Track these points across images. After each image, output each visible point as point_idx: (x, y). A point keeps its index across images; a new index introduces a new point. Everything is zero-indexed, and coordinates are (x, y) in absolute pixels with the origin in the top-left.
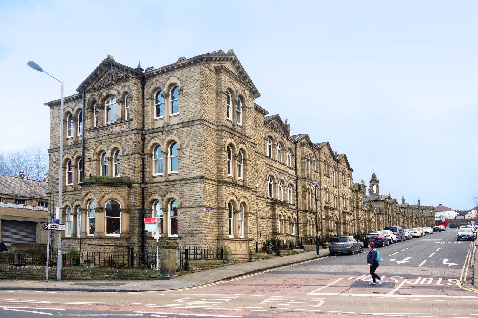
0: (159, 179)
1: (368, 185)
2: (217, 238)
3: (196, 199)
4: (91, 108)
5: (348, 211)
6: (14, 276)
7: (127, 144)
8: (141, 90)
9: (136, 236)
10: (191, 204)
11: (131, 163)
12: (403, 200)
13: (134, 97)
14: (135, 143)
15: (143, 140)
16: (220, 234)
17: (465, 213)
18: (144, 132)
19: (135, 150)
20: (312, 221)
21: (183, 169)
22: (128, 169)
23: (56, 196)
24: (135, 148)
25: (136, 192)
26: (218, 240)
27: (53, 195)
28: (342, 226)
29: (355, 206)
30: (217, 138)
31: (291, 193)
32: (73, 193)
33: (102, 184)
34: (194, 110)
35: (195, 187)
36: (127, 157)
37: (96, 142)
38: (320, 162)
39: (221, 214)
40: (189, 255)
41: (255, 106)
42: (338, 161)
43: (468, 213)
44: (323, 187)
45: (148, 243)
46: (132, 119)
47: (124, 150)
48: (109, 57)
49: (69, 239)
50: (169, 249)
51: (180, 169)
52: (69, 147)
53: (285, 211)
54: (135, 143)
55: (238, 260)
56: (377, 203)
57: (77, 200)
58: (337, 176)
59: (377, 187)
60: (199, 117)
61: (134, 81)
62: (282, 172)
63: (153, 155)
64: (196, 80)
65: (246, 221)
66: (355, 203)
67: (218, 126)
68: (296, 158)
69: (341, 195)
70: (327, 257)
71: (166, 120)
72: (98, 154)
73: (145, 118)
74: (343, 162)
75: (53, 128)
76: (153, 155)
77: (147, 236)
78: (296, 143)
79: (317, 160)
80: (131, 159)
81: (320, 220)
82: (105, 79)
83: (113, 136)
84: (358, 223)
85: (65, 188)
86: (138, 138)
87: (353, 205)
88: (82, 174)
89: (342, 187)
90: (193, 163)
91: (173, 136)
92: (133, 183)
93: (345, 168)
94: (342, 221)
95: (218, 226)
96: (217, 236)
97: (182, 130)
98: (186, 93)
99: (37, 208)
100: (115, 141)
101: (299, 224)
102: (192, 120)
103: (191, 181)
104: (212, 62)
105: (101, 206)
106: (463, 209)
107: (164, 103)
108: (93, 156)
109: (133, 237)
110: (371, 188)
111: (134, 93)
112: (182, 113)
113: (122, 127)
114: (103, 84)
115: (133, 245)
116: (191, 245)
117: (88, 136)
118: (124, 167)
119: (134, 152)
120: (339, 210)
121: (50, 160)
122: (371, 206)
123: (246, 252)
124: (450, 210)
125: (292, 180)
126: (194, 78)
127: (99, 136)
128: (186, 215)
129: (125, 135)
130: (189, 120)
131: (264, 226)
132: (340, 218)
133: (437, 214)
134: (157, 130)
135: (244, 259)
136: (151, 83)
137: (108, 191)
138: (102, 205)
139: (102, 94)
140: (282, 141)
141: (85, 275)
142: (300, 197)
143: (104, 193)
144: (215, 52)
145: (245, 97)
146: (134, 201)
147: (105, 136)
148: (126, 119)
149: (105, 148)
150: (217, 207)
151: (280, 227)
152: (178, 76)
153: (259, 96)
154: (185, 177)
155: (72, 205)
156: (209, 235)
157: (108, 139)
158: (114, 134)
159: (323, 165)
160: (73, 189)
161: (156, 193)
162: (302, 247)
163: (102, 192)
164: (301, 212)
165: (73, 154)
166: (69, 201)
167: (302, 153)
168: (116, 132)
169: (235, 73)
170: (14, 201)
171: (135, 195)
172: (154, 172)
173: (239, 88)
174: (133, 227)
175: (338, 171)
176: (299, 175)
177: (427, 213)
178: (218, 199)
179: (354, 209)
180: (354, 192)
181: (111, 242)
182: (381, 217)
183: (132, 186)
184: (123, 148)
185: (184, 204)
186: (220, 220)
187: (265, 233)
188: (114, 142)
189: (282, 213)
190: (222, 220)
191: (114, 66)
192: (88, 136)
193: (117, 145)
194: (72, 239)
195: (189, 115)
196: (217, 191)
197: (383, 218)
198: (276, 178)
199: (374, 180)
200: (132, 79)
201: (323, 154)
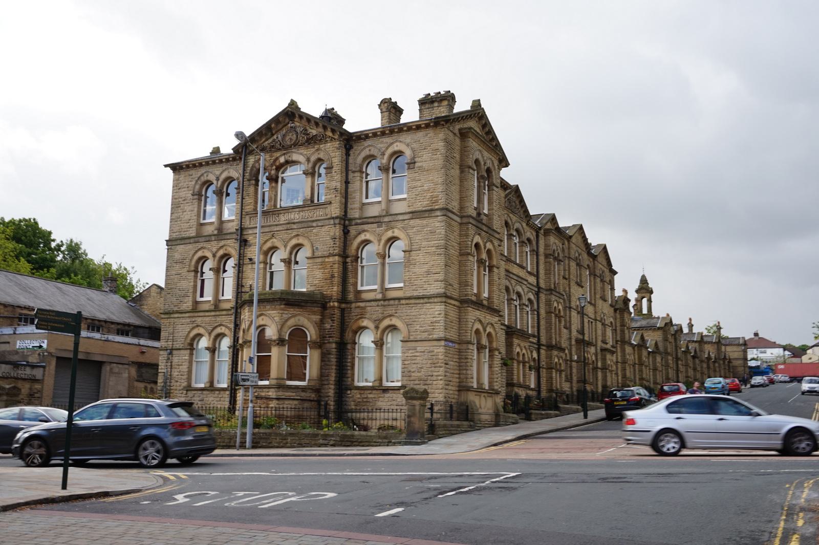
0: (371, 296)
1: (633, 296)
2: (457, 389)
5: (608, 346)
8: (345, 157)
9: (332, 384)
12: (691, 326)
13: (334, 169)
15: (346, 232)
16: (463, 382)
17: (803, 350)
18: (347, 222)
19: (334, 250)
20: (560, 364)
21: (412, 282)
23: (178, 318)
25: (334, 314)
26: (459, 391)
27: (172, 316)
28: (600, 374)
29: (619, 338)
30: (460, 235)
31: (530, 316)
32: (213, 313)
33: (284, 302)
35: (432, 310)
38: (569, 261)
39: (464, 351)
41: (501, 182)
42: (594, 257)
43: (808, 352)
44: (573, 305)
45: (350, 395)
48: (292, 101)
49: (202, 390)
51: (409, 282)
52: (207, 239)
53: (525, 347)
56: (650, 331)
57: (220, 325)
58: (593, 283)
59: (650, 301)
61: (337, 144)
62: (520, 280)
63: (359, 257)
65: (491, 363)
66: (618, 332)
67: (462, 217)
68: (537, 255)
69: (598, 319)
70: (516, 443)
71: (383, 205)
73: (349, 200)
74: (601, 259)
75: (176, 206)
76: (359, 257)
78: (537, 230)
79: (566, 257)
81: (569, 362)
82: (284, 136)
83: (295, 226)
84: (624, 369)
85: (194, 304)
86: (337, 231)
87: (616, 335)
89: (600, 303)
90: (428, 273)
91: (396, 230)
93: (605, 269)
94: (600, 365)
95: (460, 370)
96: (457, 384)
97: (412, 222)
98: (419, 167)
99: (106, 336)
100: (299, 233)
101: (541, 369)
103: (426, 300)
104: (456, 123)
105: (282, 337)
106: (797, 344)
110: (639, 304)
112: (412, 197)
113: (312, 213)
114: (280, 144)
115: (327, 399)
120: (596, 346)
122: (642, 338)
123: (491, 411)
124: (773, 345)
125: (532, 293)
126: (434, 146)
127: (268, 224)
128: (417, 352)
130: (424, 209)
132: (597, 359)
133: (752, 353)
134: (370, 220)
136: (362, 147)
139: (277, 159)
140: (521, 228)
141: (289, 440)
142: (543, 322)
143: (287, 316)
145: (493, 170)
146: (330, 329)
147: (281, 225)
150: (457, 339)
151: (519, 373)
152: (408, 140)
153: (507, 165)
154: (415, 294)
158: (297, 223)
159: (573, 264)
160: (212, 308)
161: (365, 318)
162: (557, 408)
163: (284, 316)
164: (544, 348)
166: (227, 327)
167: (547, 246)
169: (478, 130)
171: (332, 320)
172: (368, 285)
173: (487, 158)
175: (595, 275)
176: (542, 285)
177: (733, 353)
178: (460, 329)
179: (617, 343)
180: (618, 312)
181: (294, 394)
182: (659, 359)
183: (328, 305)
185: (412, 335)
186: (463, 360)
188: (298, 235)
189: (522, 350)
190: (466, 361)
194: (208, 390)
196: (459, 315)
197: (662, 360)
198: (512, 291)
199: (645, 289)
201: (574, 246)
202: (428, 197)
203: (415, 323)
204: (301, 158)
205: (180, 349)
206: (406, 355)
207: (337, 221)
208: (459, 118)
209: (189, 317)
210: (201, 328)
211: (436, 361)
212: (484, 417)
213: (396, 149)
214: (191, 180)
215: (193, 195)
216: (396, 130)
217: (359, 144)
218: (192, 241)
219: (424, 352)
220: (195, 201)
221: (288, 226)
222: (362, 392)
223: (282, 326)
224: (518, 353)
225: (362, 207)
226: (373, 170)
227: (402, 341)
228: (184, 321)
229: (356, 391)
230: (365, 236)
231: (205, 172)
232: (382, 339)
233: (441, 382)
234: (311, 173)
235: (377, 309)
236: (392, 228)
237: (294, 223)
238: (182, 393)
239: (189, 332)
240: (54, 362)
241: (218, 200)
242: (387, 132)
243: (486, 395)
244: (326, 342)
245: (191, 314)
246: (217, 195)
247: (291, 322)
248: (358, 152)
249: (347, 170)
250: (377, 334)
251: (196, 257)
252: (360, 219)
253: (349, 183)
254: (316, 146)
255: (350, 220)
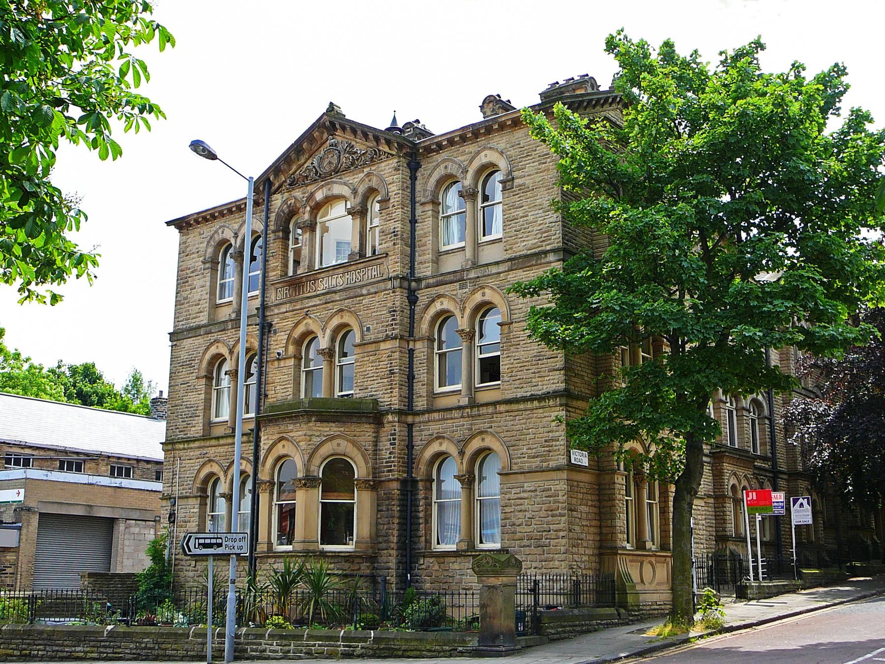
3: (547, 449)
4: (283, 231)
6: (119, 653)
7: (373, 314)
8: (409, 182)
9: (393, 549)
10: (535, 463)
11: (381, 363)
13: (391, 201)
14: (394, 311)
15: (412, 300)
19: (394, 329)
21: (513, 374)
22: (375, 378)
24: (392, 325)
34: (541, 227)
36: (372, 348)
37: (294, 313)
40: (540, 596)
45: (423, 567)
46: (387, 254)
47: (365, 329)
50: (500, 578)
53: (745, 476)
54: (394, 311)
55: (648, 608)
60: (553, 243)
61: (394, 162)
64: (545, 155)
71: (469, 253)
72: (299, 343)
75: (183, 280)
77: (419, 549)
80: (383, 352)
83: (337, 297)
86: (398, 299)
88: (262, 395)
91: (487, 291)
92: (387, 412)
98: (520, 186)
102: (537, 250)
107: (464, 212)
108: (286, 347)
109: (385, 552)
111: (394, 189)
112: (510, 234)
116: (536, 570)
117: (273, 297)
118: (364, 373)
119: (390, 333)
121: (173, 359)
129: (369, 294)
130: (529, 252)
131: (699, 517)
135: (663, 607)
136: (435, 164)
137: (328, 433)
138: (314, 471)
139: (312, 194)
141: (292, 647)
144: (573, 79)
146: (390, 458)
148: (369, 253)
149: (313, 327)
152: (502, 145)
154: (519, 395)
155: (226, 472)
156: (580, 542)
157: (323, 304)
161: (444, 438)
163: (314, 439)
164: (785, 477)
165: (233, 343)
168: (345, 286)
170: (58, 463)
174: (385, 527)
184: (361, 327)
185: (516, 464)
187: (702, 537)
188: (341, 310)
189: (740, 483)
191: (344, 129)
192: (273, 297)
193: (347, 318)
195: (529, 238)
200: (387, 157)
202: (535, 233)
203: (521, 443)
204: (346, 191)
205: (187, 497)
206: (507, 496)
207: (397, 283)
208: (582, 102)
209: (199, 447)
210: (214, 464)
211: (554, 506)
212: (647, 598)
213: (484, 160)
214: (201, 239)
215: (204, 263)
216: (482, 131)
217: (430, 160)
218: (202, 331)
219: (535, 491)
220: (207, 271)
221: (328, 296)
222: (442, 560)
223: (311, 456)
224: (734, 486)
225: (437, 259)
226: (452, 200)
227: (499, 474)
228: (192, 454)
229: (432, 560)
230: (442, 303)
231: (220, 228)
232: (471, 472)
233: (564, 541)
234: (360, 212)
235: (462, 421)
236: (482, 288)
237: (335, 292)
238: (190, 565)
239: (199, 471)
240: (35, 520)
241: (237, 266)
242: (469, 135)
243: (653, 559)
244: (383, 479)
245: (202, 443)
246: (236, 260)
247: (326, 450)
248: (429, 172)
249: (413, 202)
250: (462, 463)
251: (208, 356)
252: (433, 277)
253: (416, 222)
254: (365, 170)
255: (419, 280)
